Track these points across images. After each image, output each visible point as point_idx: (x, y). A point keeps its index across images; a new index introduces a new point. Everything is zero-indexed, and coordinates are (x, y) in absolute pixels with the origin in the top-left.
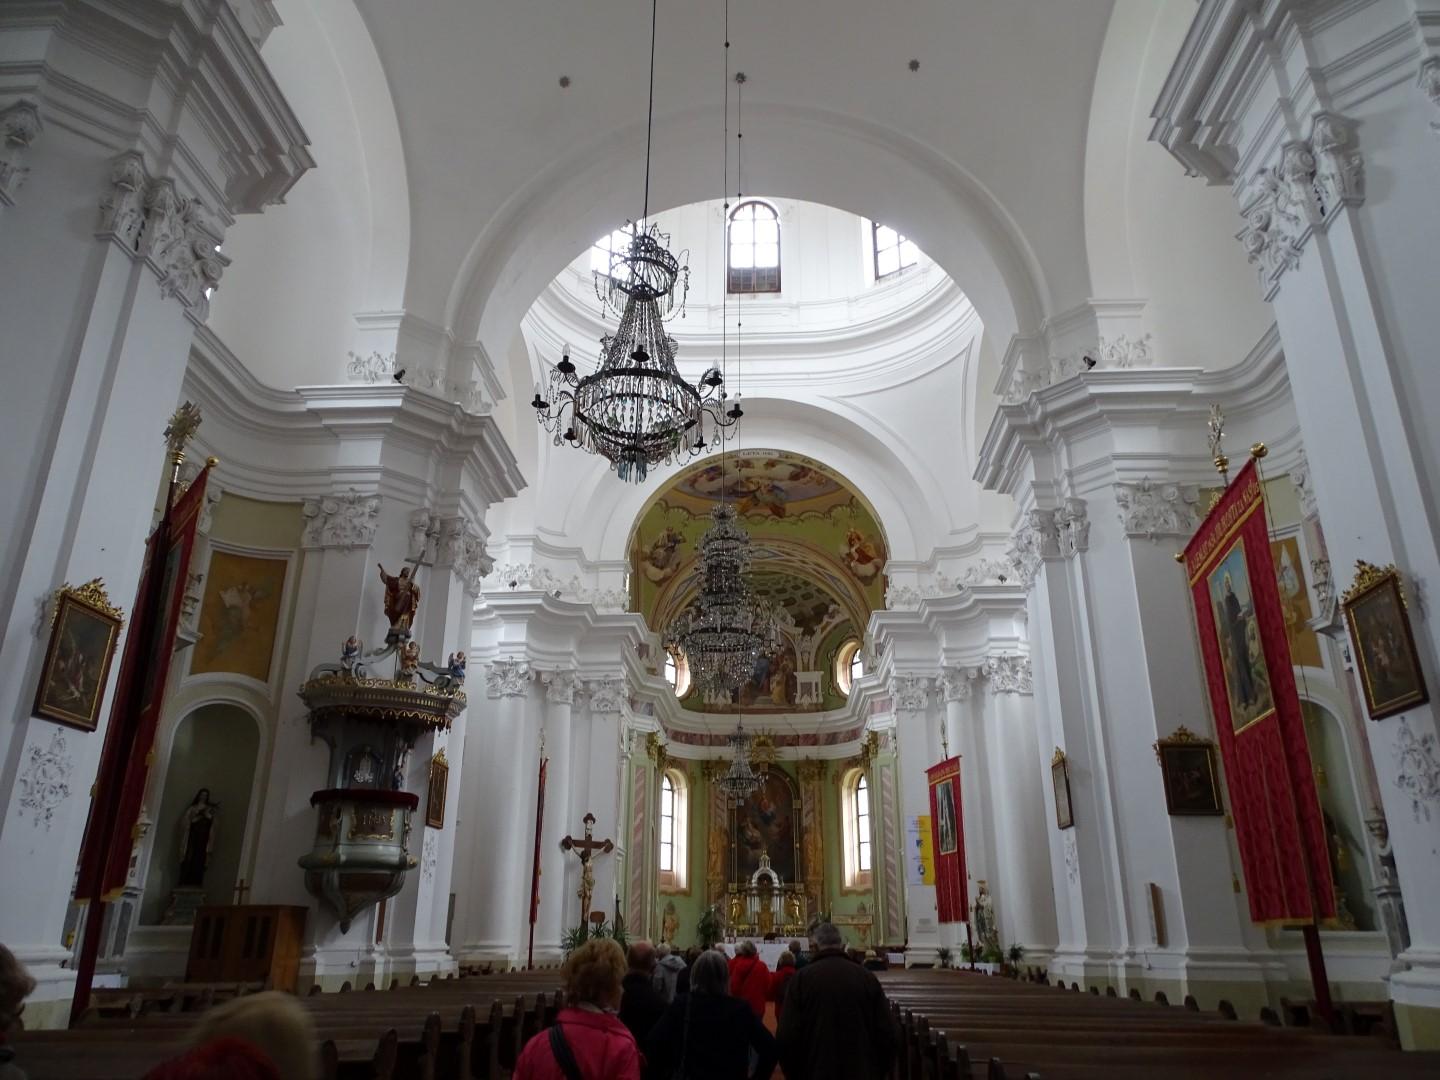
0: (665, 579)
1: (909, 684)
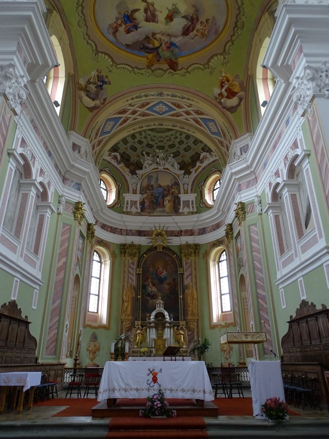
1: (324, 74)
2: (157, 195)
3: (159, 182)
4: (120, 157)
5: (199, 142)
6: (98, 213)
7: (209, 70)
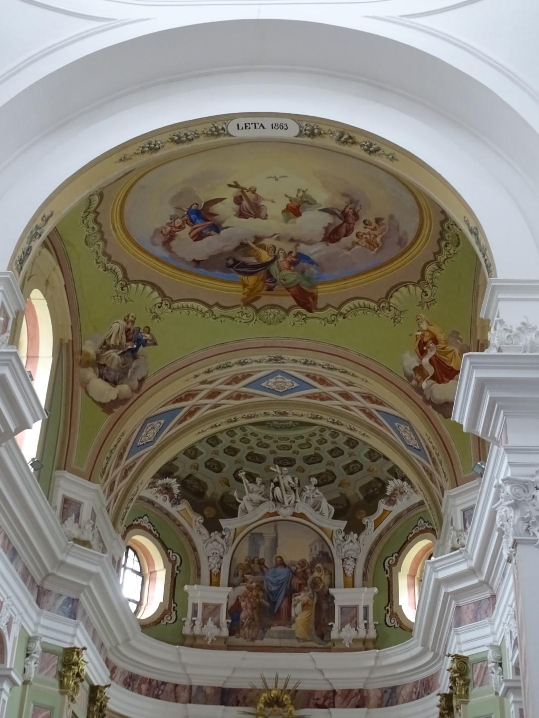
0: (119, 401)
2: (274, 588)
3: (280, 552)
4: (179, 488)
5: (380, 457)
6: (119, 651)
7: (391, 314)
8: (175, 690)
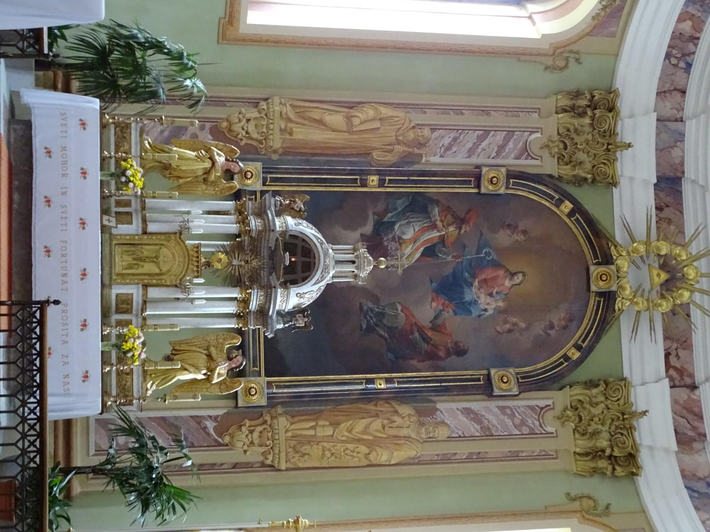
8: (675, 89)
